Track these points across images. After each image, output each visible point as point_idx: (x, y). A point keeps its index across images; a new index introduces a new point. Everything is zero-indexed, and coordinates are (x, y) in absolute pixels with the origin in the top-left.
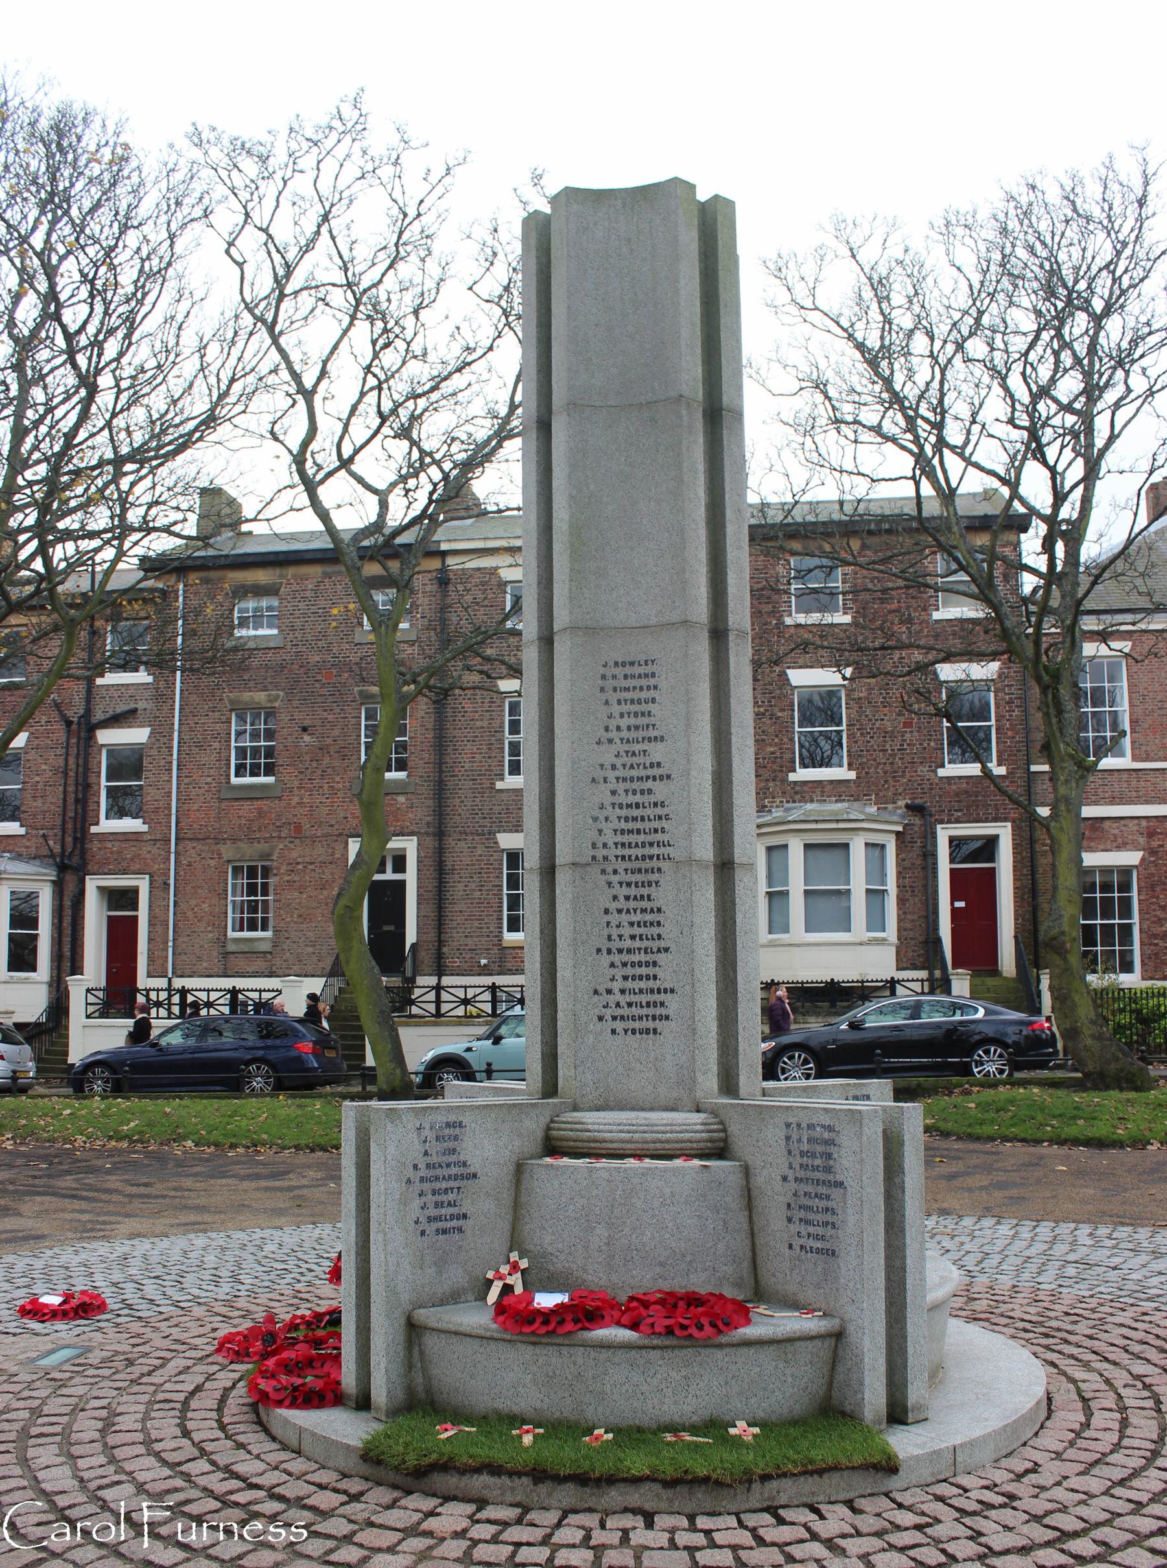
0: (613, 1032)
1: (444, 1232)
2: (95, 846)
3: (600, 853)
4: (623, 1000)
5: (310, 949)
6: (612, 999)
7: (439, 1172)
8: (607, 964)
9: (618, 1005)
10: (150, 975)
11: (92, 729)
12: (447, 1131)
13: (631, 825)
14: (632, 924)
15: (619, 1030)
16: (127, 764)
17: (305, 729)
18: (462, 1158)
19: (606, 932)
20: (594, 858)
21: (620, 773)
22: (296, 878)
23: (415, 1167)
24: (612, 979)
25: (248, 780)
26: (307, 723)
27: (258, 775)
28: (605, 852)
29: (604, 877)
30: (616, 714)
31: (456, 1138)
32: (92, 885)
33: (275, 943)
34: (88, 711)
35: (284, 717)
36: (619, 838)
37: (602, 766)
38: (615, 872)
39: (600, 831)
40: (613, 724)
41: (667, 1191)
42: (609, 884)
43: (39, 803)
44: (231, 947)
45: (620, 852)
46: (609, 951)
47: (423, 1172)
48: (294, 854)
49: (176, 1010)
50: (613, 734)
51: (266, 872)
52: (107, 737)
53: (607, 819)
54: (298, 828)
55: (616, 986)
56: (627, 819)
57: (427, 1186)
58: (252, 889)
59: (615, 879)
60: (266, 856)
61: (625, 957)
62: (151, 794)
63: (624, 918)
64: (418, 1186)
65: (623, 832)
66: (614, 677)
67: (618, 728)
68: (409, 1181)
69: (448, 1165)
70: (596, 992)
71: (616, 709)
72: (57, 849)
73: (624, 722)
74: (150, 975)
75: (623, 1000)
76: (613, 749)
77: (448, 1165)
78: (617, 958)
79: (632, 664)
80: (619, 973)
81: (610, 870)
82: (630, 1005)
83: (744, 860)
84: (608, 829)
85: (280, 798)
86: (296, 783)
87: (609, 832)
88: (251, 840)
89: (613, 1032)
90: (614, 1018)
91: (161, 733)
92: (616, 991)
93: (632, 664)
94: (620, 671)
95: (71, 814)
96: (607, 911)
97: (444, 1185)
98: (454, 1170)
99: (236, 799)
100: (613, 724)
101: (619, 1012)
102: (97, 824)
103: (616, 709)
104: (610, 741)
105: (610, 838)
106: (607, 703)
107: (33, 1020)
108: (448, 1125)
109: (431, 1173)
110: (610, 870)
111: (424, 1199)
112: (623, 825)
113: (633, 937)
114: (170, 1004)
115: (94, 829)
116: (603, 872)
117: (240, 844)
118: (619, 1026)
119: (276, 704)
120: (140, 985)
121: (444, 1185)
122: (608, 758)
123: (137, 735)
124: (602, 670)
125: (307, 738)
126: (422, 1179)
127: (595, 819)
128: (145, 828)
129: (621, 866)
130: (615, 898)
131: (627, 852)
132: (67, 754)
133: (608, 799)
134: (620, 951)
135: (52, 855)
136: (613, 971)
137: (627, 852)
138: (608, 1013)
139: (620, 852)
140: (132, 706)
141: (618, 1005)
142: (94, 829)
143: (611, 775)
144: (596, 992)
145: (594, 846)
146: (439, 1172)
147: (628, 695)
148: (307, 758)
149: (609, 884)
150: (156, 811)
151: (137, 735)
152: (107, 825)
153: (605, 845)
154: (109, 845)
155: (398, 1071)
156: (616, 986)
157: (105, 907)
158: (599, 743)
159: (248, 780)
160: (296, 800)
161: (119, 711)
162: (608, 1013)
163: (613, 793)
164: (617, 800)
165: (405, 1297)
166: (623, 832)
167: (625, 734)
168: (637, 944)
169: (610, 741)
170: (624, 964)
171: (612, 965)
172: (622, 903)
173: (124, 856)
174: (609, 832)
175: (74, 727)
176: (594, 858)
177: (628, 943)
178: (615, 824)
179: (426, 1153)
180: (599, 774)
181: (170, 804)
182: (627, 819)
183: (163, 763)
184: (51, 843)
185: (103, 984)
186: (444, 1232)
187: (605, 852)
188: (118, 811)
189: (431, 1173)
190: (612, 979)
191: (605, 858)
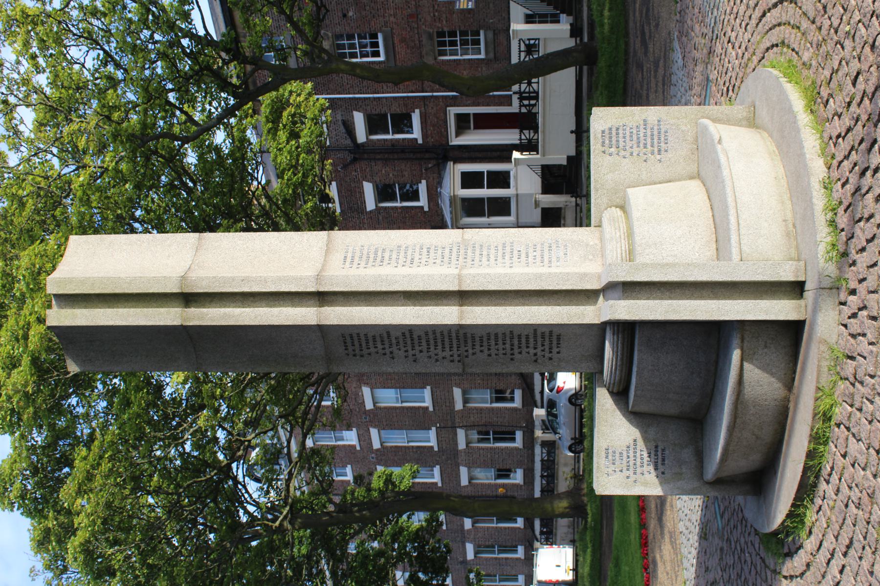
0: (558, 353)
1: (663, 460)
2: (431, 140)
3: (456, 358)
4: (540, 348)
5: (491, 5)
6: (539, 353)
7: (631, 463)
8: (520, 356)
9: (543, 351)
10: (510, 105)
11: (357, 146)
12: (610, 457)
13: (440, 344)
14: (496, 344)
15: (557, 350)
16: (375, 124)
17: (345, 16)
18: (625, 449)
19: (501, 356)
20: (459, 361)
21: (409, 348)
22: (444, 16)
23: (628, 477)
24: (528, 353)
25: (381, 49)
26: (340, 14)
27: (378, 42)
28: (456, 356)
29: (470, 356)
30: (376, 350)
31: (614, 452)
32: (455, 141)
33: (487, 28)
34: (345, 149)
35: (338, 30)
36: (447, 349)
37: (406, 357)
38: (467, 351)
39: (443, 358)
40: (381, 351)
41: (650, 367)
42: (474, 354)
43: (406, 173)
44: (491, 55)
45: (455, 349)
46: (512, 354)
47: (631, 472)
48: (429, 19)
49: (533, 102)
50: (388, 351)
51: (441, 34)
52: (361, 136)
53: (436, 355)
54: (411, 16)
55: (532, 351)
56: (436, 346)
57: (639, 470)
58: (453, 44)
59: (471, 351)
60: (430, 37)
61: (516, 347)
62: (397, 109)
63: (493, 347)
64: (639, 476)
65: (444, 348)
66: (354, 350)
67: (384, 349)
68: (635, 482)
69: (628, 457)
70: (536, 361)
71: (372, 350)
72: (433, 162)
73: (380, 346)
74: (510, 105)
75: (540, 348)
76: (396, 351)
77: (628, 457)
78: (516, 351)
79: (345, 343)
80: (525, 350)
81: (466, 354)
82: (543, 345)
83: (456, 282)
84: (442, 355)
85: (392, 29)
86: (381, 19)
87: (444, 354)
88: (421, 46)
89: (558, 353)
90: (551, 352)
91: (356, 105)
92: (535, 351)
93: (345, 343)
94: (350, 348)
95: (411, 156)
96: (490, 355)
97: (638, 460)
98: (631, 454)
99: (395, 56)
100: (381, 351)
101: (547, 350)
102: (416, 140)
103: (372, 350)
104: (391, 353)
105: (447, 353)
106: (369, 354)
107: (540, 180)
108: (607, 457)
109: (631, 469)
110: (466, 354)
111: (645, 473)
112: (440, 347)
113: (504, 344)
114: (529, 105)
115: (420, 141)
116: (467, 357)
117: (424, 53)
118: (555, 350)
119: (330, 35)
120: (517, 111)
121: (638, 460)
122: (402, 353)
123: (359, 119)
124: (351, 356)
125: (351, 14)
126: (635, 473)
127: (437, 360)
128: (417, 111)
129: (463, 349)
130: (481, 351)
131: (455, 346)
132: (375, 159)
133: (425, 353)
134: (512, 349)
135: (438, 165)
136: (524, 353)
137: (455, 346)
138: (547, 355)
139: (455, 349)
140: (340, 123)
141: (543, 351)
142: (420, 141)
143: (411, 352)
144: (536, 361)
145: (452, 361)
146: (631, 463)
147: (364, 345)
148: (364, 13)
149: (474, 354)
150: (406, 105)
151: (359, 119)
152: (416, 134)
153: (451, 356)
154: (429, 132)
155: (575, 54)
156: (532, 351)
157: (468, 131)
158: (393, 358)
159: (381, 49)
160: (392, 19)
161: (344, 131)
162: (547, 355)
163: (421, 351)
164: (425, 350)
165: (696, 484)
166: (444, 348)
167: (387, 346)
168: (508, 342)
169: (391, 353)
170: (520, 347)
171: (520, 353)
172: (485, 349)
173: (434, 124)
174: (444, 354)
175: (357, 156)
176: (459, 361)
177: (508, 346)
178: (439, 351)
179: (621, 471)
180: (411, 358)
181: (401, 97)
182: (436, 346)
183: (375, 103)
184: (430, 166)
185: (517, 131)
186: (663, 460)
187: (456, 356)
188: (415, 196)
189: (631, 469)
190: (528, 353)
191: (459, 356)
